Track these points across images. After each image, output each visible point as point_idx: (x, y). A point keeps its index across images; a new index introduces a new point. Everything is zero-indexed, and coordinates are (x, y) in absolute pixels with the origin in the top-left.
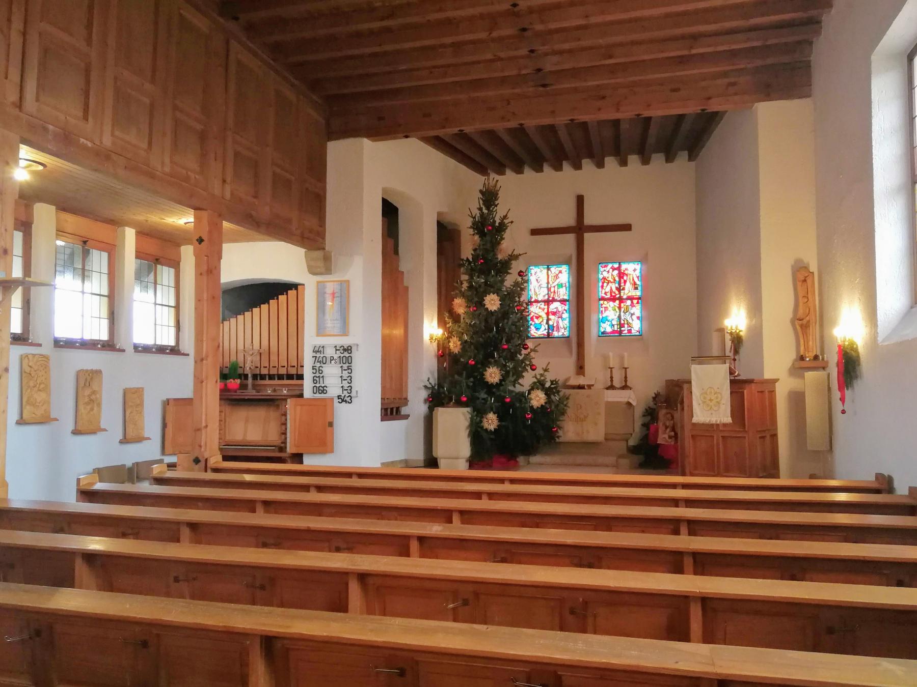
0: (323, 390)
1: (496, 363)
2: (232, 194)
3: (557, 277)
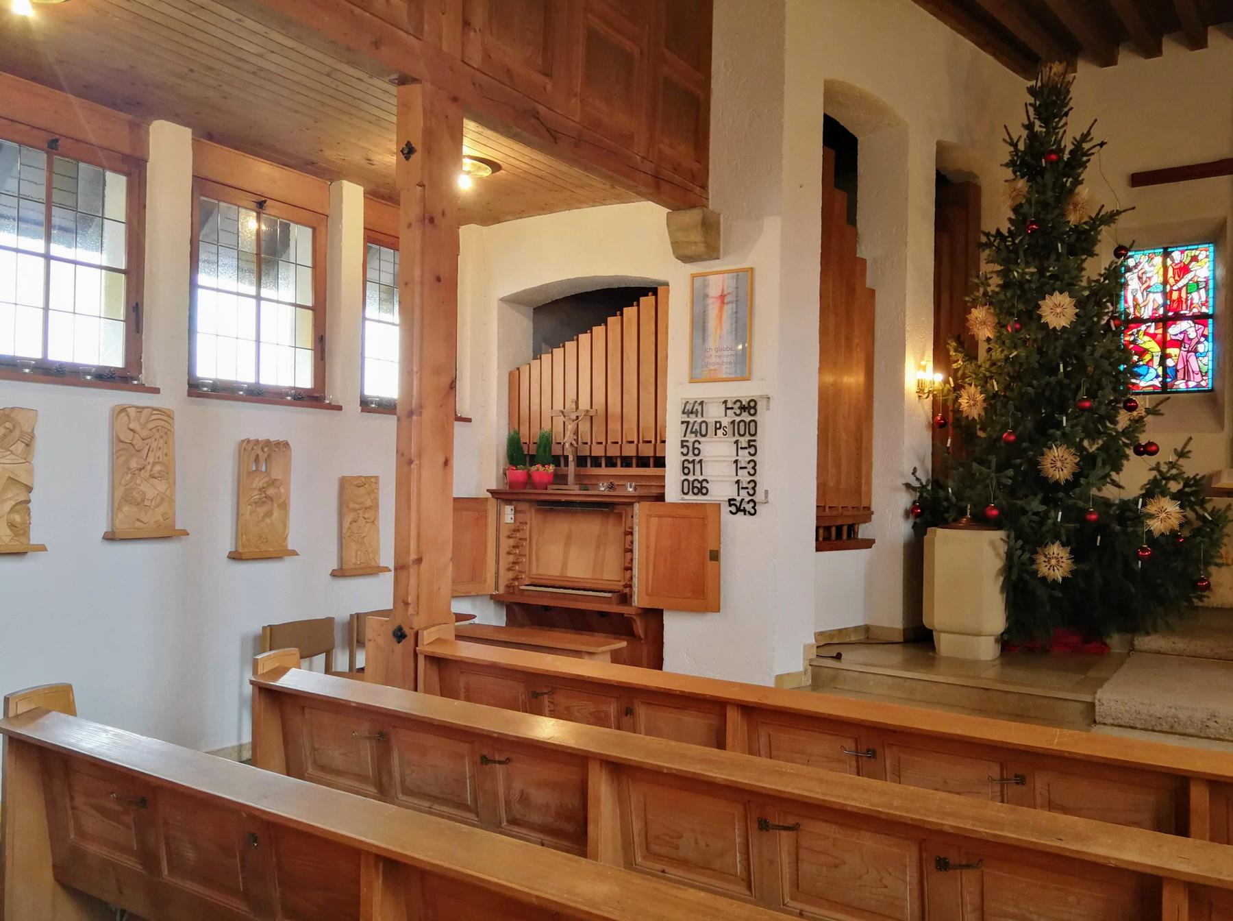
0: (700, 488)
1: (1067, 440)
2: (487, 56)
3: (1185, 269)
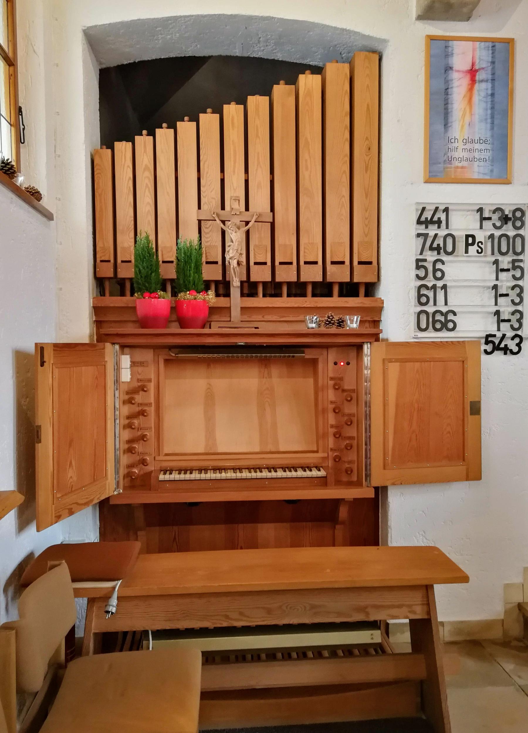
0: (444, 321)
